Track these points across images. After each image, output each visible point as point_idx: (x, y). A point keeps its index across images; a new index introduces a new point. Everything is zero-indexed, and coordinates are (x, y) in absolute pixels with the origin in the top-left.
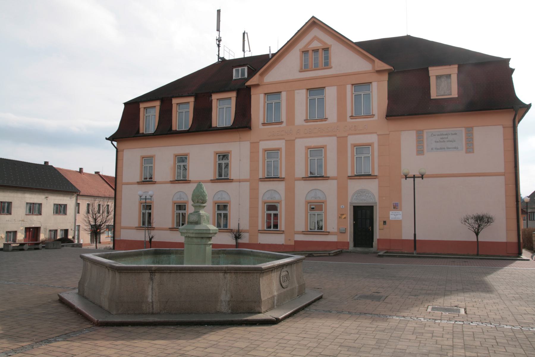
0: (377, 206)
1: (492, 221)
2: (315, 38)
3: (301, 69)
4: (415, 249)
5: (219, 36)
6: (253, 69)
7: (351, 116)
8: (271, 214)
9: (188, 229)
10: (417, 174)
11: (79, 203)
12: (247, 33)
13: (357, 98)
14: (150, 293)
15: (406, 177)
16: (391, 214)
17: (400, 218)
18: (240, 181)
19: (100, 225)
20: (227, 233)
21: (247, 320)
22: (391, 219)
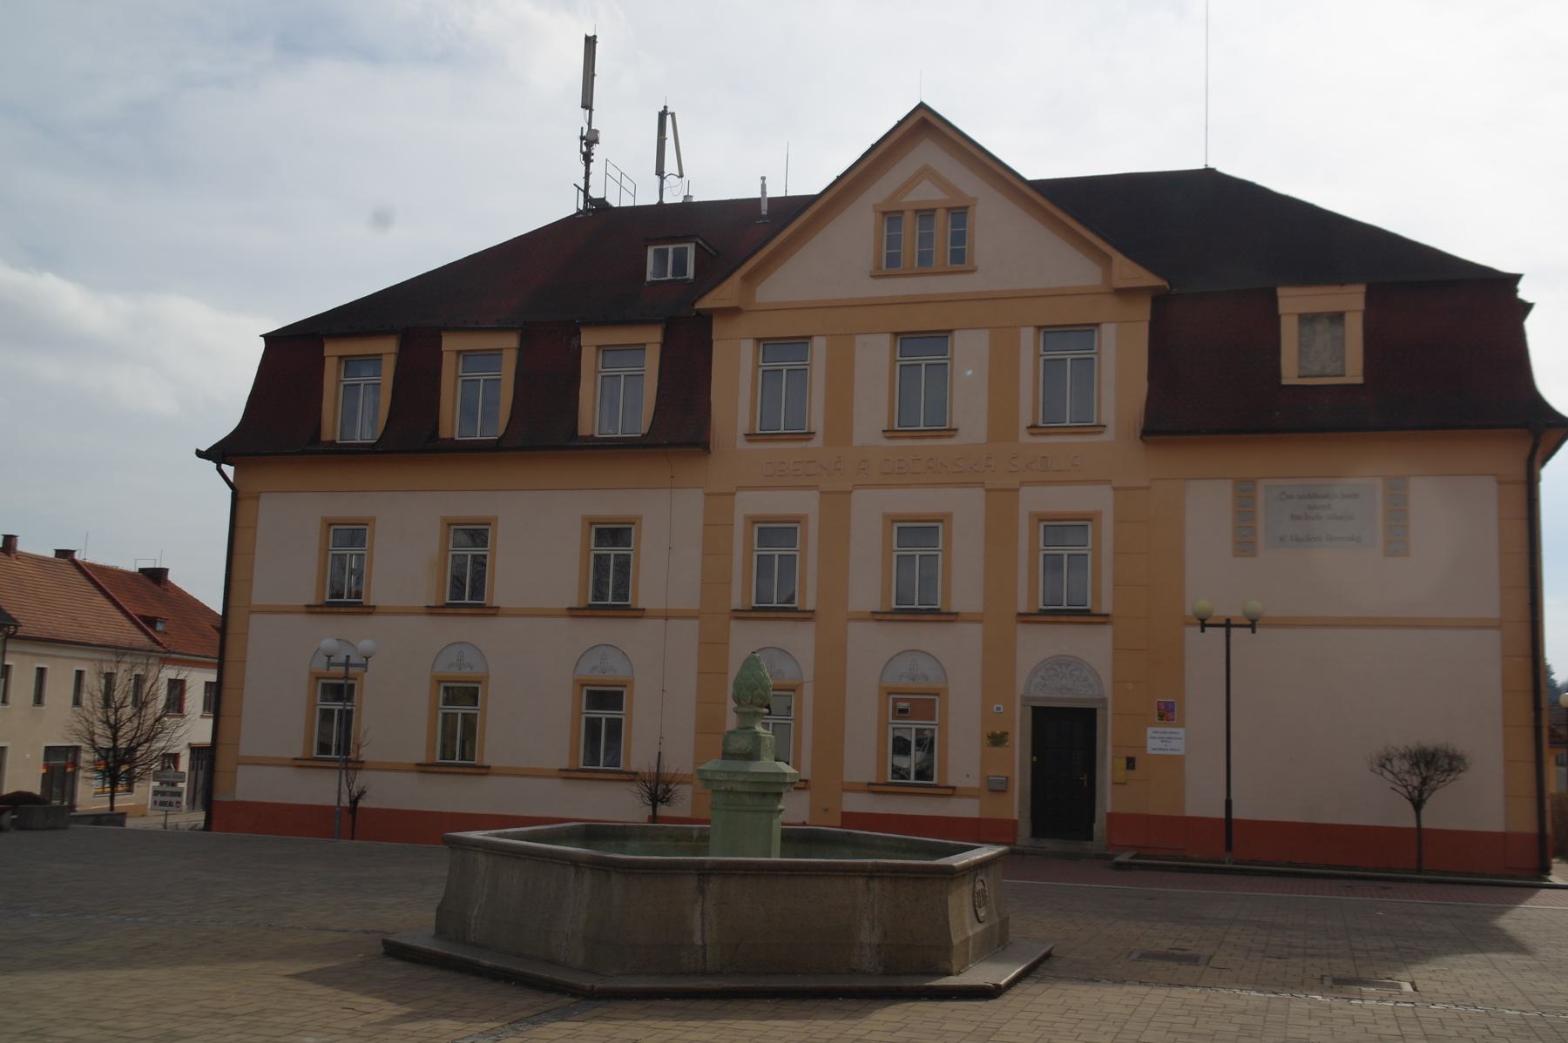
0: (1106, 709)
1: (1462, 768)
2: (926, 173)
3: (879, 267)
4: (1229, 847)
5: (590, 124)
6: (711, 251)
7: (1033, 427)
8: (601, 719)
9: (731, 772)
10: (1235, 613)
11: (8, 666)
12: (673, 115)
13: (1052, 369)
14: (697, 923)
15: (1203, 624)
16: (1151, 738)
17: (1178, 750)
18: (667, 616)
19: (131, 750)
20: (622, 786)
21: (933, 986)
22: (1150, 751)
